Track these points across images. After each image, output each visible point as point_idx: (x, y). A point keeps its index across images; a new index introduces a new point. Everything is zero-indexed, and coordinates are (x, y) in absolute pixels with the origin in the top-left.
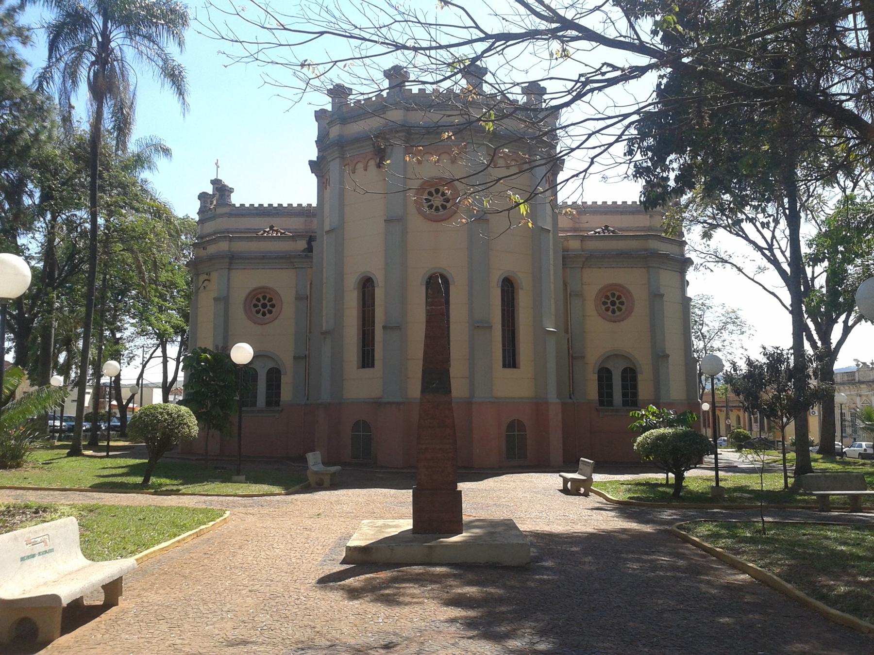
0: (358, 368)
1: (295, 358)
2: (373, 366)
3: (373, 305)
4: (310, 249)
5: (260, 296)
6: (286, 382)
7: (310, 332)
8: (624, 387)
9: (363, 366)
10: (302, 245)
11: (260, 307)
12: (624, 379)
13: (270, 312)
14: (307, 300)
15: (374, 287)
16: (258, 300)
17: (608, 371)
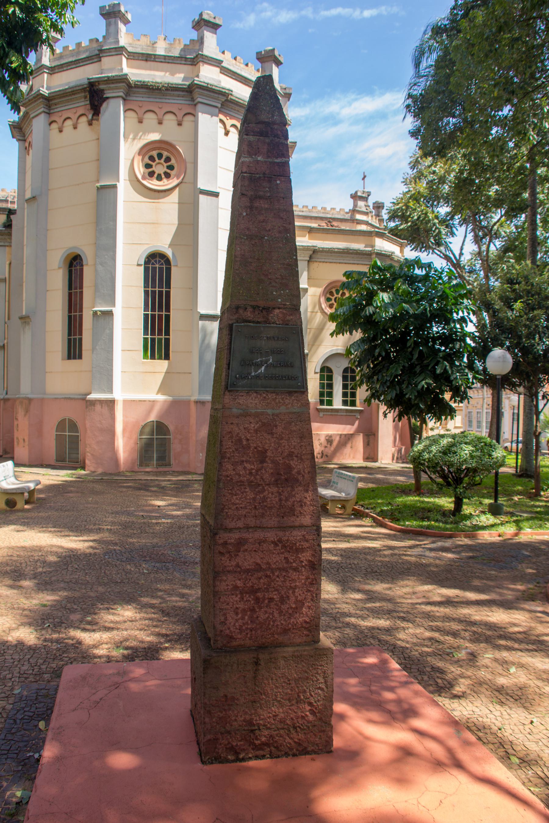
0: (63, 359)
2: (80, 357)
3: (81, 287)
7: (9, 319)
9: (69, 358)
15: (82, 265)
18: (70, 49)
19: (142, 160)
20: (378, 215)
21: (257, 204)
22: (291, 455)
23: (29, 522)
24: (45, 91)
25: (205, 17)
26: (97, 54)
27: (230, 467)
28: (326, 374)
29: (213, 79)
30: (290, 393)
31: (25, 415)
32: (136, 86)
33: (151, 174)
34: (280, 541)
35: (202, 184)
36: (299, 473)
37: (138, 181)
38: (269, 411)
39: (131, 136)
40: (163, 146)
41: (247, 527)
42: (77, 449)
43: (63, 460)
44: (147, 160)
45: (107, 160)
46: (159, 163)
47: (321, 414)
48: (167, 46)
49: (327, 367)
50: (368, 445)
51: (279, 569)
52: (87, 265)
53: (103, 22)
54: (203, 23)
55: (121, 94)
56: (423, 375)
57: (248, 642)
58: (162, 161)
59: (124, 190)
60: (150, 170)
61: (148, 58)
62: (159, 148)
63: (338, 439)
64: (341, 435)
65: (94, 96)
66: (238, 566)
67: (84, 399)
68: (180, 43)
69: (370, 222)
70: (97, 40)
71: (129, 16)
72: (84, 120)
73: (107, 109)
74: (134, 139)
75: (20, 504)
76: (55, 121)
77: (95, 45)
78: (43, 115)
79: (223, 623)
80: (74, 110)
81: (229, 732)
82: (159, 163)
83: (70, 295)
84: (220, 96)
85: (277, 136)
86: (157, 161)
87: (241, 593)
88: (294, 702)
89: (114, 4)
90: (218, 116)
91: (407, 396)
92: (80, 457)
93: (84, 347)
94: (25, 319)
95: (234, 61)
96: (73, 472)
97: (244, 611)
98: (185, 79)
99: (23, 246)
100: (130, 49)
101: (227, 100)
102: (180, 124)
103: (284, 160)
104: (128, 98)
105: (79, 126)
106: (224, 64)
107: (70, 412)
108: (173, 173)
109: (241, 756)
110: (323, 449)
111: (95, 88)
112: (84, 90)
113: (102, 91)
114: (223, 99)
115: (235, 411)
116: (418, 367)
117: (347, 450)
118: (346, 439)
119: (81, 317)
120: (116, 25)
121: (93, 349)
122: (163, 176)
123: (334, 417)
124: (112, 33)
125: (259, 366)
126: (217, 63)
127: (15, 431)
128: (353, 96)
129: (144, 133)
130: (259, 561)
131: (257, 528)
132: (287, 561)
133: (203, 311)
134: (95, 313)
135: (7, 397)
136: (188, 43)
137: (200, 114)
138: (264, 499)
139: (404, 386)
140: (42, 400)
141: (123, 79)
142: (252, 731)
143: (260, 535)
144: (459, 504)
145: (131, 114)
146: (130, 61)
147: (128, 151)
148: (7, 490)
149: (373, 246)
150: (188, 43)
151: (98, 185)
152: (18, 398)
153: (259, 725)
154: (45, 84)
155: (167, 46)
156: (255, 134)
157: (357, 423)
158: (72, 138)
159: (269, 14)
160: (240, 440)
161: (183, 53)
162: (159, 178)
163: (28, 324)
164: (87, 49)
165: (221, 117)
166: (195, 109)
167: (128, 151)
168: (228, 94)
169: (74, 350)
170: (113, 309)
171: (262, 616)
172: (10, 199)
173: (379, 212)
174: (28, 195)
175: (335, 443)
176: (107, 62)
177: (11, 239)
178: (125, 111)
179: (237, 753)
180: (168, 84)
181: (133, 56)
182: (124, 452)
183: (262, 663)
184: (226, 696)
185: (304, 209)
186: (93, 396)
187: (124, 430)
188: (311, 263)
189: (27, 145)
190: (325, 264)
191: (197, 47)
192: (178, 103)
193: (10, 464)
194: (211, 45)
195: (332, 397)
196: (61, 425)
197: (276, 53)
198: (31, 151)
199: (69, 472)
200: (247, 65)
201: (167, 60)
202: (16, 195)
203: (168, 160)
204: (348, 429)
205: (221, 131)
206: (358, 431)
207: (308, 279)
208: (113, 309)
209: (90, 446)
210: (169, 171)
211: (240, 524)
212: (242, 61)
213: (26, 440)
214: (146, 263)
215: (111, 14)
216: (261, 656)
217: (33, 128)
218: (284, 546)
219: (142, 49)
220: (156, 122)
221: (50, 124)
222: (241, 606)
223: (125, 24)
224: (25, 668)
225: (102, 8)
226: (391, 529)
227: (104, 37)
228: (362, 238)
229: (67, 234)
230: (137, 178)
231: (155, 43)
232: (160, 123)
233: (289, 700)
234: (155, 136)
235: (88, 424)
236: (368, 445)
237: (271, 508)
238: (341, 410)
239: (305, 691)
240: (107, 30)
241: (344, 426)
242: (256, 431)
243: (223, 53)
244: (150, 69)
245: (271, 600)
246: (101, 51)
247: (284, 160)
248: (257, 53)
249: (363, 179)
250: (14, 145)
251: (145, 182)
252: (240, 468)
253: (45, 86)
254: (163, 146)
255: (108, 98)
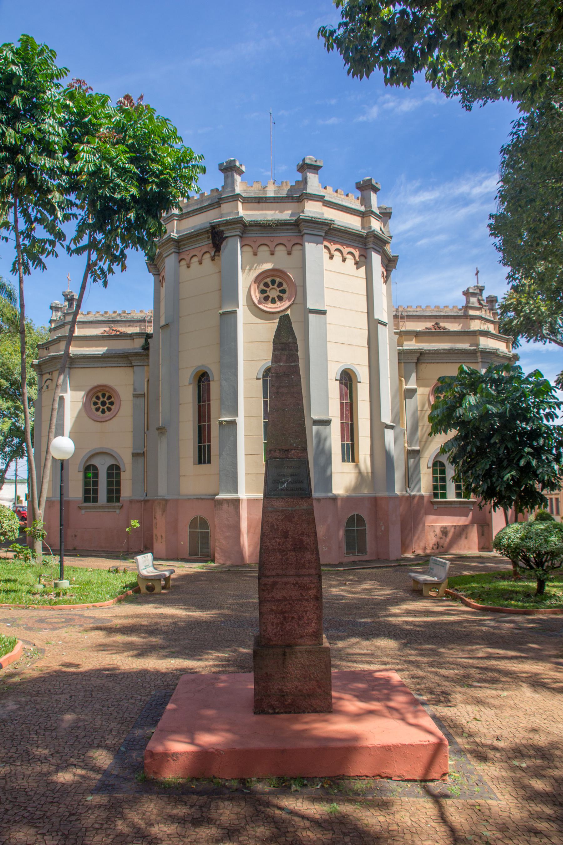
0: (194, 464)
1: (134, 455)
2: (209, 462)
3: (209, 400)
4: (146, 348)
5: (100, 395)
6: (126, 478)
7: (148, 429)
8: (109, 483)
9: (200, 463)
10: (139, 342)
11: (102, 407)
12: (109, 475)
13: (109, 409)
14: (145, 398)
15: (209, 381)
16: (98, 398)
17: (95, 468)
18: (195, 198)
19: (258, 287)
20: (491, 309)
21: (280, 391)
22: (303, 533)
23: (163, 602)
24: (175, 235)
25: (308, 161)
26: (217, 201)
27: (267, 541)
28: (438, 468)
29: (317, 212)
30: (302, 498)
31: (162, 515)
32: (251, 225)
33: (266, 299)
34: (297, 583)
35: (310, 305)
36: (307, 544)
37: (255, 305)
38: (290, 509)
39: (248, 268)
40: (276, 273)
41: (278, 575)
42: (208, 543)
43: (196, 554)
44: (262, 287)
45: (229, 290)
46: (272, 289)
47: (435, 507)
48: (276, 189)
49: (440, 462)
50: (483, 535)
51: (298, 600)
52: (213, 380)
53: (222, 175)
54: (306, 167)
55: (238, 233)
56: (510, 468)
57: (280, 643)
58: (275, 286)
59: (243, 313)
60: (265, 295)
61: (260, 201)
62: (272, 276)
63: (453, 530)
64: (455, 526)
65: (216, 237)
66: (273, 597)
67: (213, 499)
68: (287, 185)
69: (483, 316)
70: (217, 190)
71: (243, 168)
72: (207, 256)
73: (226, 246)
74: (250, 270)
75: (158, 589)
76: (184, 259)
77: (215, 194)
78: (173, 255)
79: (265, 631)
80: (199, 249)
81: (269, 696)
82: (272, 289)
83: (199, 407)
84: (324, 226)
85: (291, 350)
86: (271, 286)
87: (275, 614)
88: (307, 679)
89: (231, 161)
90: (322, 244)
91: (498, 489)
92: (211, 551)
93: (212, 453)
94: (161, 430)
95: (335, 194)
96: (205, 564)
97: (277, 624)
98: (292, 215)
99: (159, 365)
100: (244, 195)
101: (330, 229)
102: (289, 254)
103: (296, 363)
104: (244, 236)
105: (204, 262)
106: (326, 199)
107: (201, 511)
108: (285, 296)
109: (277, 711)
110: (438, 540)
111: (216, 230)
112: (207, 232)
113: (222, 232)
114: (326, 228)
115: (270, 509)
116: (506, 461)
117: (463, 542)
118: (461, 532)
119: (209, 426)
120: (233, 177)
121: (220, 455)
122: (277, 299)
123: (449, 509)
124: (229, 183)
125: (283, 483)
126: (320, 198)
127: (154, 529)
128: (484, 175)
129: (259, 264)
130: (285, 595)
131: (283, 575)
132: (302, 596)
133: (316, 417)
134: (221, 423)
135: (146, 498)
136: (294, 184)
137: (306, 244)
138: (287, 559)
139: (494, 480)
140: (177, 500)
141: (239, 221)
142: (283, 696)
143: (285, 579)
144: (541, 585)
145: (246, 248)
146: (245, 204)
147: (245, 281)
148: (147, 576)
149: (478, 345)
150: (294, 184)
151: (221, 311)
152: (157, 499)
153: (287, 692)
154: (175, 229)
155: (276, 189)
156: (278, 350)
157: (471, 514)
158: (198, 272)
159: (391, 105)
160: (273, 526)
161: (289, 193)
162: (273, 301)
163: (164, 434)
164: (209, 197)
165: (326, 243)
166: (302, 239)
167: (245, 281)
168: (331, 224)
169: (203, 456)
170: (237, 419)
171: (288, 628)
172: (147, 319)
173: (493, 306)
174: (162, 323)
175: (450, 535)
176: (226, 207)
177: (148, 359)
178: (242, 247)
179: (274, 709)
180: (278, 220)
181: (247, 201)
182: (249, 546)
183: (287, 654)
184: (267, 673)
185: (418, 309)
186: (221, 496)
187: (249, 526)
188: (419, 365)
189: (161, 278)
190: (432, 365)
191: (302, 187)
192: (287, 236)
193: (149, 556)
194: (314, 184)
195: (445, 490)
196: (193, 523)
197: (374, 182)
198: (164, 284)
199: (201, 564)
200: (347, 195)
201: (276, 200)
202: (152, 315)
203: (280, 285)
204: (462, 521)
205: (326, 255)
206: (473, 522)
207: (417, 379)
208: (237, 419)
209: (219, 540)
210: (281, 295)
211: (274, 573)
212: (343, 193)
213: (164, 536)
214: (264, 376)
215: (229, 169)
216: (287, 650)
217: (166, 264)
218: (299, 587)
219: (255, 194)
220: (268, 253)
221: (180, 261)
222: (275, 621)
223: (240, 175)
224: (159, 682)
225: (220, 165)
226: (474, 607)
227: (223, 187)
228: (466, 338)
229: (196, 354)
230: (254, 303)
231: (266, 187)
232: (272, 254)
233: (305, 678)
234: (268, 266)
235: (217, 521)
236: (483, 535)
237: (291, 564)
238: (454, 502)
239: (314, 673)
240: (225, 182)
241: (458, 518)
242: (282, 520)
243: (325, 188)
244: (262, 210)
245: (293, 618)
246: (220, 199)
247: (296, 363)
248: (356, 184)
249: (477, 274)
250: (151, 277)
251: (261, 306)
252: (273, 541)
253: (175, 231)
254: (276, 273)
255: (227, 237)
